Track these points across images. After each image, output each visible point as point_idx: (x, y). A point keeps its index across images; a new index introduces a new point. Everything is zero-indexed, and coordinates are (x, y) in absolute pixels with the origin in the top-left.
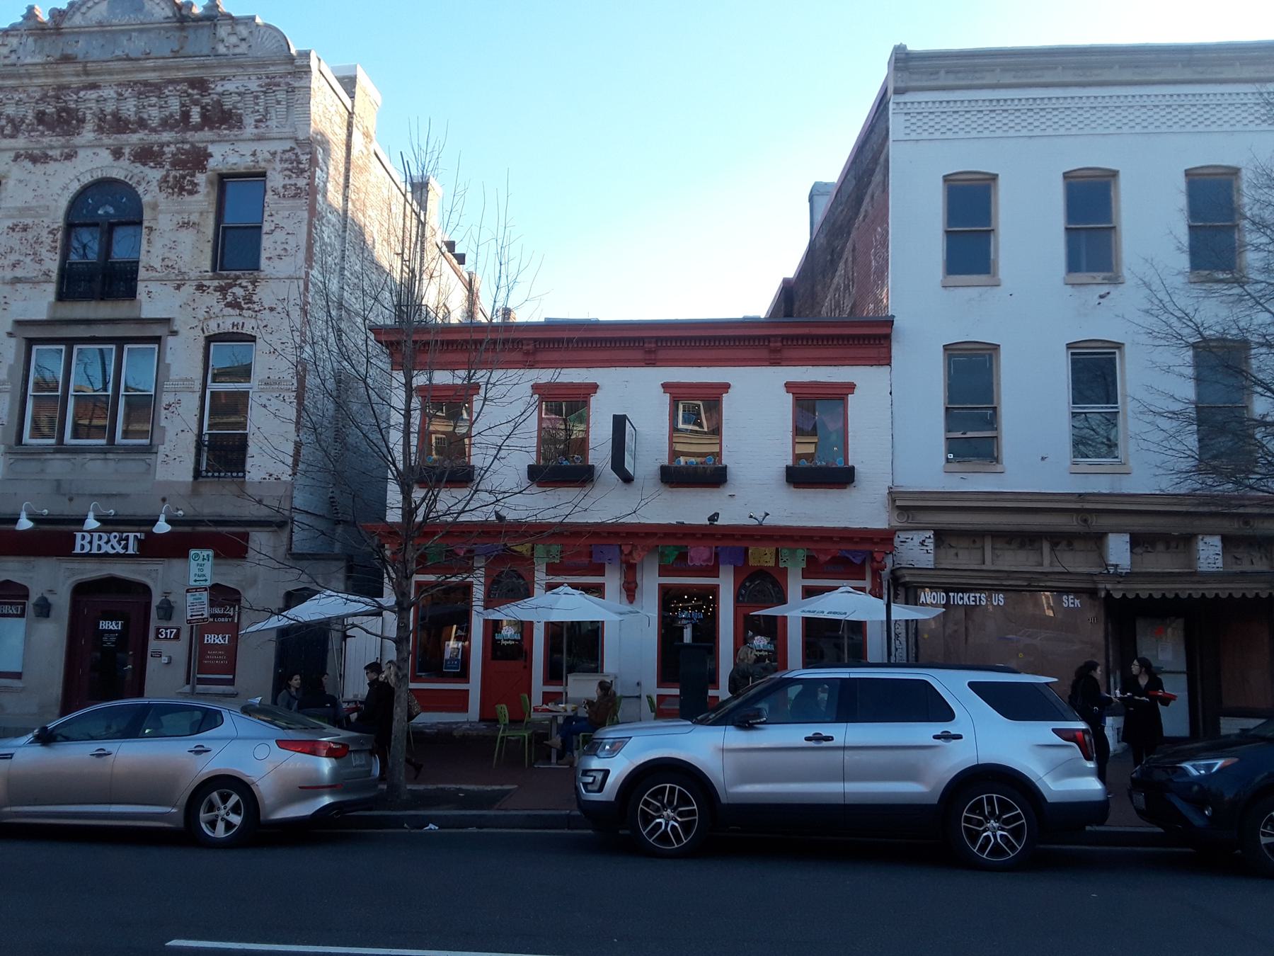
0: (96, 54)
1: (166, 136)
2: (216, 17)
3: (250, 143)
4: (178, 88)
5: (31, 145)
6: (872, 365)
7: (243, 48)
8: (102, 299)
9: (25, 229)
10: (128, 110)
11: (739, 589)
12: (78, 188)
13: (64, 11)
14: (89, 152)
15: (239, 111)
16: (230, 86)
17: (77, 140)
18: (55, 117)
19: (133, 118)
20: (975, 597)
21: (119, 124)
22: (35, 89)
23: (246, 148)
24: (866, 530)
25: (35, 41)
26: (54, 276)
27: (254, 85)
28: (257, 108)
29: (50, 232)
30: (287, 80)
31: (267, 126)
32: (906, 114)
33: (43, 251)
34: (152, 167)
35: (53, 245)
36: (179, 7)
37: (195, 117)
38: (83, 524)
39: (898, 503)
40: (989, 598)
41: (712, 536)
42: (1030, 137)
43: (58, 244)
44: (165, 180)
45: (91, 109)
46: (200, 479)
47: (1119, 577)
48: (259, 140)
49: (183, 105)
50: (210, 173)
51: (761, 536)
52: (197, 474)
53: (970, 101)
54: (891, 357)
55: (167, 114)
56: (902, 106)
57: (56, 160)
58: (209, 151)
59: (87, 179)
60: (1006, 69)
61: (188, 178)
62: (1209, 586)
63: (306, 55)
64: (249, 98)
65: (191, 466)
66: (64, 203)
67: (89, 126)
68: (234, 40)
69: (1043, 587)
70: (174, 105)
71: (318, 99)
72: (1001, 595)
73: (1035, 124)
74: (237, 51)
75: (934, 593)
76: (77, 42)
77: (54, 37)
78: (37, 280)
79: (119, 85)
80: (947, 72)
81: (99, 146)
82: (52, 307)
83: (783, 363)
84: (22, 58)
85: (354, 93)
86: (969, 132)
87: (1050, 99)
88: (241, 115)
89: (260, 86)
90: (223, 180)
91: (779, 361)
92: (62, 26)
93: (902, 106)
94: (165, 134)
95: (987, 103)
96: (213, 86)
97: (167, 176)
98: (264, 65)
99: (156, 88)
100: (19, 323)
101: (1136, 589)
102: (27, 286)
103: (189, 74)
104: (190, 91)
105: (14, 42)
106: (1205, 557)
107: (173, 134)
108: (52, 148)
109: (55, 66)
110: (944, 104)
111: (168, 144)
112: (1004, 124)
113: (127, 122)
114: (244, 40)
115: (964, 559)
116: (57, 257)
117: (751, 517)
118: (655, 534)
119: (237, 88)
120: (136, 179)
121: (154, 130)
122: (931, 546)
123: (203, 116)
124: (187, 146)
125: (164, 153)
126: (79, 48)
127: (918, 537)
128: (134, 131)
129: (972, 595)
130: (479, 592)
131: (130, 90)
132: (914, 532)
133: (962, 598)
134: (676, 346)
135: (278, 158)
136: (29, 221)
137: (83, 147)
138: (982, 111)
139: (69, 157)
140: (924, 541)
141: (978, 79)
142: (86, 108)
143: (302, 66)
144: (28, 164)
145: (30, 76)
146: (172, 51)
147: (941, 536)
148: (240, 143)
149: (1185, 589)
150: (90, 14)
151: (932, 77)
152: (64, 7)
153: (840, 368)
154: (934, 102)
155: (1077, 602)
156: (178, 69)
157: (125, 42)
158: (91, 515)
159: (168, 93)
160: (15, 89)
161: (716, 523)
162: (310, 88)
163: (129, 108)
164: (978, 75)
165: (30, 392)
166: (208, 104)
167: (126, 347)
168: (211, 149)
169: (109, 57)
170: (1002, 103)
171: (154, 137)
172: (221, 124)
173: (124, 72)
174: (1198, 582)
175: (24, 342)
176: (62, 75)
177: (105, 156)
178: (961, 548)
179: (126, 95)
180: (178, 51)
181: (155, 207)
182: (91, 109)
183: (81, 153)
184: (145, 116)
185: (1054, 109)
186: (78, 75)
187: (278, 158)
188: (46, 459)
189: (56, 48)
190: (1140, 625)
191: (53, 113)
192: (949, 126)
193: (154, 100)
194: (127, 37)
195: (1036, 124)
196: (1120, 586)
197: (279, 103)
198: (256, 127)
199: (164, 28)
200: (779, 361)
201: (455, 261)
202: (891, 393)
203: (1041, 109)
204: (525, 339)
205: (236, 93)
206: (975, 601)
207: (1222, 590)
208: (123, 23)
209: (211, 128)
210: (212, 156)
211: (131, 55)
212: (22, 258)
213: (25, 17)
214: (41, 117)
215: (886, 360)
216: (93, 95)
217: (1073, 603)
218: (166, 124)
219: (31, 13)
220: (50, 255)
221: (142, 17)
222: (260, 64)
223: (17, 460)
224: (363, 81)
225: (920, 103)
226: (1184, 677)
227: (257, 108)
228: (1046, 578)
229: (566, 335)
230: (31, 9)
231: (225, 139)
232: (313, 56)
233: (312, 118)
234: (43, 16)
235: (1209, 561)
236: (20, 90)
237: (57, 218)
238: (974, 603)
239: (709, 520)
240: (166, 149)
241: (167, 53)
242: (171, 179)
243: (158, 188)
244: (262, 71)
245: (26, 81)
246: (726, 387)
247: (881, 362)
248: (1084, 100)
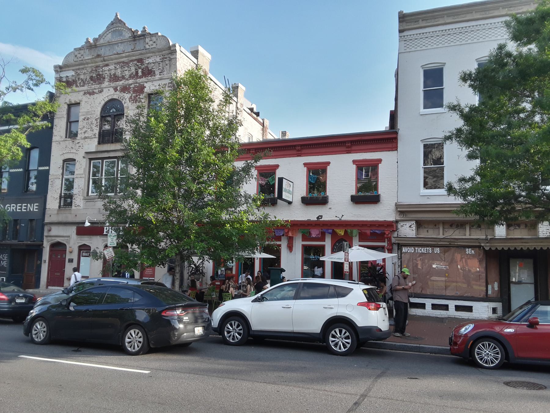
0: (108, 53)
1: (131, 81)
2: (145, 35)
3: (158, 81)
4: (134, 63)
5: (89, 89)
6: (389, 151)
7: (154, 46)
8: (112, 143)
9: (88, 119)
10: (118, 73)
11: (333, 246)
12: (104, 103)
13: (97, 39)
14: (107, 89)
15: (154, 70)
16: (150, 60)
17: (103, 85)
18: (96, 78)
19: (120, 76)
20: (427, 249)
21: (115, 78)
22: (89, 68)
23: (156, 83)
24: (385, 222)
25: (89, 51)
26: (97, 136)
27: (158, 59)
28: (160, 67)
29: (95, 120)
30: (169, 56)
31: (163, 74)
32: (405, 41)
33: (94, 127)
34: (127, 93)
35: (97, 124)
36: (133, 32)
37: (140, 74)
38: (84, 224)
39: (398, 210)
40: (433, 250)
41: (319, 225)
42: (461, 45)
43: (98, 124)
44: (131, 97)
45: (107, 73)
46: (61, 208)
47: (501, 240)
48: (161, 80)
49: (136, 69)
50: (145, 94)
51: (338, 224)
52: (60, 207)
53: (433, 32)
54: (397, 147)
55: (131, 73)
56: (403, 37)
57: (97, 93)
58: (145, 85)
59: (106, 99)
61: (138, 96)
62: (531, 244)
63: (174, 46)
64: (157, 64)
65: (58, 205)
66: (99, 109)
67: (106, 80)
68: (151, 43)
69: (456, 245)
70: (133, 69)
71: (180, 62)
72: (438, 249)
73: (451, 40)
74: (153, 47)
75: (409, 248)
76: (102, 49)
77: (94, 48)
78: (92, 137)
79: (115, 64)
80: (423, 20)
81: (110, 87)
82: (97, 146)
83: (352, 152)
84: (85, 57)
85: (198, 57)
87: (469, 27)
88: (155, 71)
89: (160, 59)
90: (150, 95)
91: (350, 151)
92: (97, 44)
93: (403, 37)
94: (130, 81)
95: (441, 32)
96: (145, 61)
97: (132, 96)
98: (161, 51)
99: (126, 64)
100: (87, 153)
101: (496, 246)
102: (89, 140)
103: (137, 57)
104: (138, 64)
105: (82, 52)
106: (541, 231)
107: (133, 80)
108: (95, 89)
109: (94, 59)
110: (421, 35)
111: (131, 84)
112: (449, 40)
113: (118, 77)
114: (154, 42)
115: (430, 234)
116: (98, 129)
117: (336, 217)
118: (375, 225)
119: (153, 61)
120: (122, 98)
121: (127, 80)
122: (414, 228)
123: (142, 72)
124: (137, 85)
125: (131, 88)
126: (102, 52)
127: (408, 224)
128: (121, 81)
129: (425, 248)
130: (328, 249)
131: (118, 65)
132: (407, 222)
133: (421, 250)
134: (353, 144)
135: (167, 86)
136: (89, 116)
137: (105, 88)
138: (438, 36)
139: (101, 92)
140: (411, 225)
141: (436, 21)
142: (105, 74)
143: (173, 50)
144: (88, 95)
145: (87, 63)
146: (132, 49)
147: (420, 224)
148: (155, 82)
149: (526, 245)
150: (105, 39)
151: (416, 23)
152: (97, 37)
153: (376, 153)
154: (417, 34)
155: (473, 251)
156: (133, 56)
157: (117, 48)
158: (87, 221)
159: (131, 65)
160: (83, 69)
161: (320, 220)
162: (176, 58)
163: (119, 72)
164: (437, 20)
165: (91, 177)
166: (144, 68)
167: (105, 161)
168: (145, 84)
169: (111, 54)
170: (447, 31)
171: (127, 82)
172: (149, 75)
173: (116, 59)
174: (525, 242)
175: (88, 160)
176: (97, 62)
177: (112, 90)
178: (429, 228)
179: (118, 67)
180: (133, 49)
181: (128, 108)
182: (107, 73)
183: (105, 90)
184: (124, 75)
185: (471, 31)
186: (102, 62)
187: (167, 86)
188: (96, 201)
189: (95, 53)
190: (512, 262)
191: (95, 76)
192: (424, 44)
193: (126, 68)
194: (117, 46)
195: (463, 38)
196: (488, 244)
197: (167, 65)
198: (160, 75)
199: (129, 41)
200: (350, 151)
201: (255, 116)
202: (397, 162)
203: (466, 32)
204: (297, 145)
205: (152, 63)
206: (427, 251)
207: (506, 246)
208: (116, 40)
209: (145, 77)
210: (145, 87)
211: (119, 53)
212: (87, 130)
213: (86, 43)
214: (91, 78)
215: (395, 148)
216: (106, 68)
217: (471, 252)
218: (131, 77)
219: (87, 41)
220: (96, 128)
221: (121, 38)
222: (160, 51)
223: (87, 201)
224: (201, 50)
225: (410, 35)
226: (532, 286)
227: (160, 67)
228: (457, 241)
229: (295, 144)
230: (87, 39)
231: (150, 80)
232: (177, 45)
233: (178, 69)
234: (91, 41)
235: (544, 233)
236: (85, 69)
237: (98, 114)
238: (426, 252)
239: (317, 218)
240: (131, 86)
241: (130, 50)
242: (133, 97)
243: (129, 101)
244: (161, 53)
245: (86, 66)
246: (328, 163)
247: (393, 149)
248: (486, 25)
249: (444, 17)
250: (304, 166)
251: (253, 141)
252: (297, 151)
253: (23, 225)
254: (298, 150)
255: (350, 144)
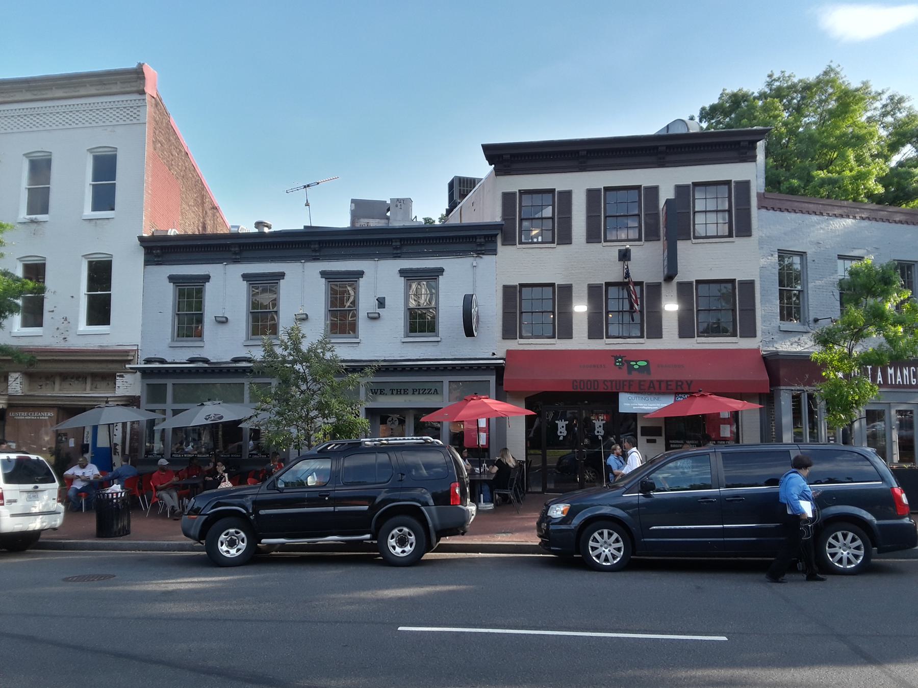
60: (102, 83)
73: (93, 119)
86: (104, 122)
91: (399, 255)
249: (52, 89)
250: (320, 276)
251: (463, 222)
252: (394, 248)
253: (447, 414)
254: (396, 248)
255: (398, 243)
